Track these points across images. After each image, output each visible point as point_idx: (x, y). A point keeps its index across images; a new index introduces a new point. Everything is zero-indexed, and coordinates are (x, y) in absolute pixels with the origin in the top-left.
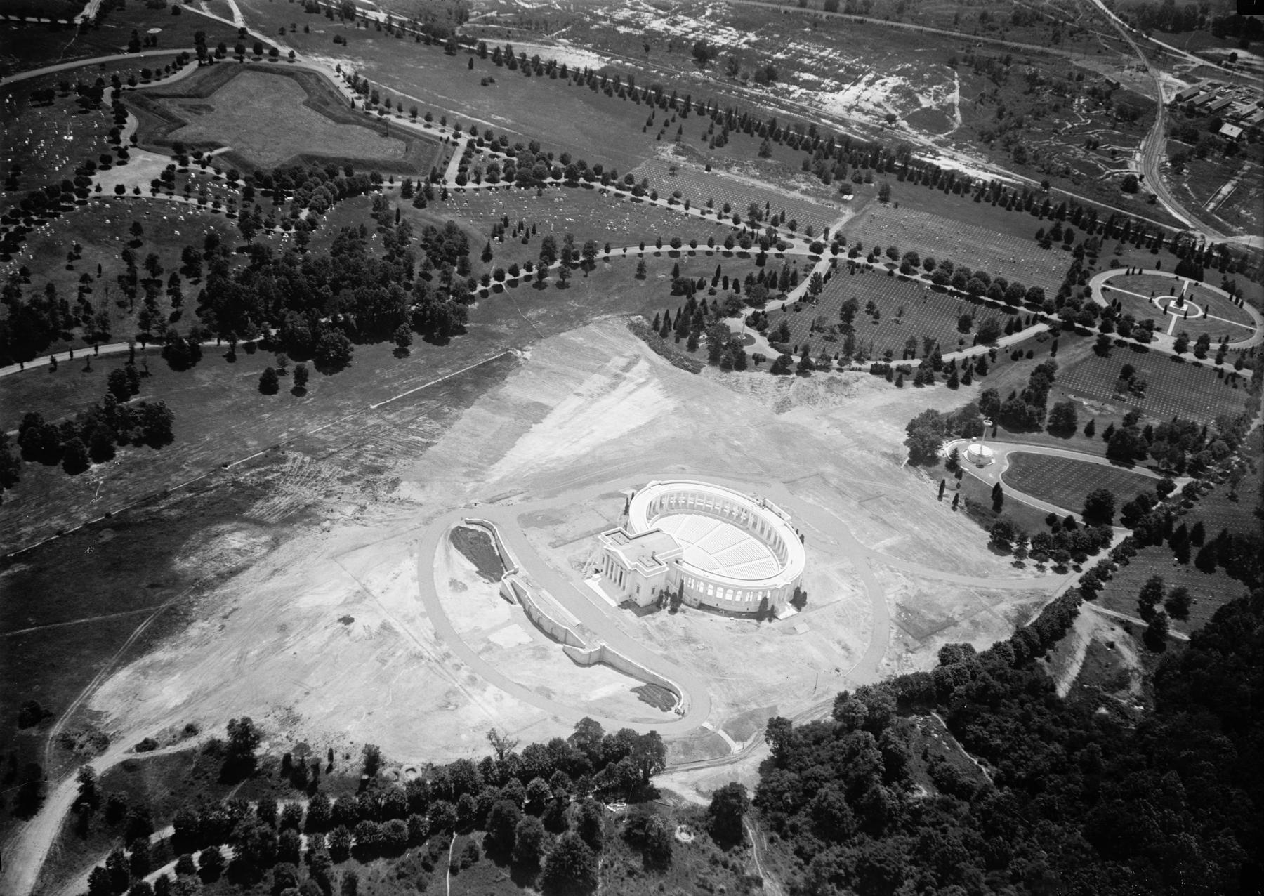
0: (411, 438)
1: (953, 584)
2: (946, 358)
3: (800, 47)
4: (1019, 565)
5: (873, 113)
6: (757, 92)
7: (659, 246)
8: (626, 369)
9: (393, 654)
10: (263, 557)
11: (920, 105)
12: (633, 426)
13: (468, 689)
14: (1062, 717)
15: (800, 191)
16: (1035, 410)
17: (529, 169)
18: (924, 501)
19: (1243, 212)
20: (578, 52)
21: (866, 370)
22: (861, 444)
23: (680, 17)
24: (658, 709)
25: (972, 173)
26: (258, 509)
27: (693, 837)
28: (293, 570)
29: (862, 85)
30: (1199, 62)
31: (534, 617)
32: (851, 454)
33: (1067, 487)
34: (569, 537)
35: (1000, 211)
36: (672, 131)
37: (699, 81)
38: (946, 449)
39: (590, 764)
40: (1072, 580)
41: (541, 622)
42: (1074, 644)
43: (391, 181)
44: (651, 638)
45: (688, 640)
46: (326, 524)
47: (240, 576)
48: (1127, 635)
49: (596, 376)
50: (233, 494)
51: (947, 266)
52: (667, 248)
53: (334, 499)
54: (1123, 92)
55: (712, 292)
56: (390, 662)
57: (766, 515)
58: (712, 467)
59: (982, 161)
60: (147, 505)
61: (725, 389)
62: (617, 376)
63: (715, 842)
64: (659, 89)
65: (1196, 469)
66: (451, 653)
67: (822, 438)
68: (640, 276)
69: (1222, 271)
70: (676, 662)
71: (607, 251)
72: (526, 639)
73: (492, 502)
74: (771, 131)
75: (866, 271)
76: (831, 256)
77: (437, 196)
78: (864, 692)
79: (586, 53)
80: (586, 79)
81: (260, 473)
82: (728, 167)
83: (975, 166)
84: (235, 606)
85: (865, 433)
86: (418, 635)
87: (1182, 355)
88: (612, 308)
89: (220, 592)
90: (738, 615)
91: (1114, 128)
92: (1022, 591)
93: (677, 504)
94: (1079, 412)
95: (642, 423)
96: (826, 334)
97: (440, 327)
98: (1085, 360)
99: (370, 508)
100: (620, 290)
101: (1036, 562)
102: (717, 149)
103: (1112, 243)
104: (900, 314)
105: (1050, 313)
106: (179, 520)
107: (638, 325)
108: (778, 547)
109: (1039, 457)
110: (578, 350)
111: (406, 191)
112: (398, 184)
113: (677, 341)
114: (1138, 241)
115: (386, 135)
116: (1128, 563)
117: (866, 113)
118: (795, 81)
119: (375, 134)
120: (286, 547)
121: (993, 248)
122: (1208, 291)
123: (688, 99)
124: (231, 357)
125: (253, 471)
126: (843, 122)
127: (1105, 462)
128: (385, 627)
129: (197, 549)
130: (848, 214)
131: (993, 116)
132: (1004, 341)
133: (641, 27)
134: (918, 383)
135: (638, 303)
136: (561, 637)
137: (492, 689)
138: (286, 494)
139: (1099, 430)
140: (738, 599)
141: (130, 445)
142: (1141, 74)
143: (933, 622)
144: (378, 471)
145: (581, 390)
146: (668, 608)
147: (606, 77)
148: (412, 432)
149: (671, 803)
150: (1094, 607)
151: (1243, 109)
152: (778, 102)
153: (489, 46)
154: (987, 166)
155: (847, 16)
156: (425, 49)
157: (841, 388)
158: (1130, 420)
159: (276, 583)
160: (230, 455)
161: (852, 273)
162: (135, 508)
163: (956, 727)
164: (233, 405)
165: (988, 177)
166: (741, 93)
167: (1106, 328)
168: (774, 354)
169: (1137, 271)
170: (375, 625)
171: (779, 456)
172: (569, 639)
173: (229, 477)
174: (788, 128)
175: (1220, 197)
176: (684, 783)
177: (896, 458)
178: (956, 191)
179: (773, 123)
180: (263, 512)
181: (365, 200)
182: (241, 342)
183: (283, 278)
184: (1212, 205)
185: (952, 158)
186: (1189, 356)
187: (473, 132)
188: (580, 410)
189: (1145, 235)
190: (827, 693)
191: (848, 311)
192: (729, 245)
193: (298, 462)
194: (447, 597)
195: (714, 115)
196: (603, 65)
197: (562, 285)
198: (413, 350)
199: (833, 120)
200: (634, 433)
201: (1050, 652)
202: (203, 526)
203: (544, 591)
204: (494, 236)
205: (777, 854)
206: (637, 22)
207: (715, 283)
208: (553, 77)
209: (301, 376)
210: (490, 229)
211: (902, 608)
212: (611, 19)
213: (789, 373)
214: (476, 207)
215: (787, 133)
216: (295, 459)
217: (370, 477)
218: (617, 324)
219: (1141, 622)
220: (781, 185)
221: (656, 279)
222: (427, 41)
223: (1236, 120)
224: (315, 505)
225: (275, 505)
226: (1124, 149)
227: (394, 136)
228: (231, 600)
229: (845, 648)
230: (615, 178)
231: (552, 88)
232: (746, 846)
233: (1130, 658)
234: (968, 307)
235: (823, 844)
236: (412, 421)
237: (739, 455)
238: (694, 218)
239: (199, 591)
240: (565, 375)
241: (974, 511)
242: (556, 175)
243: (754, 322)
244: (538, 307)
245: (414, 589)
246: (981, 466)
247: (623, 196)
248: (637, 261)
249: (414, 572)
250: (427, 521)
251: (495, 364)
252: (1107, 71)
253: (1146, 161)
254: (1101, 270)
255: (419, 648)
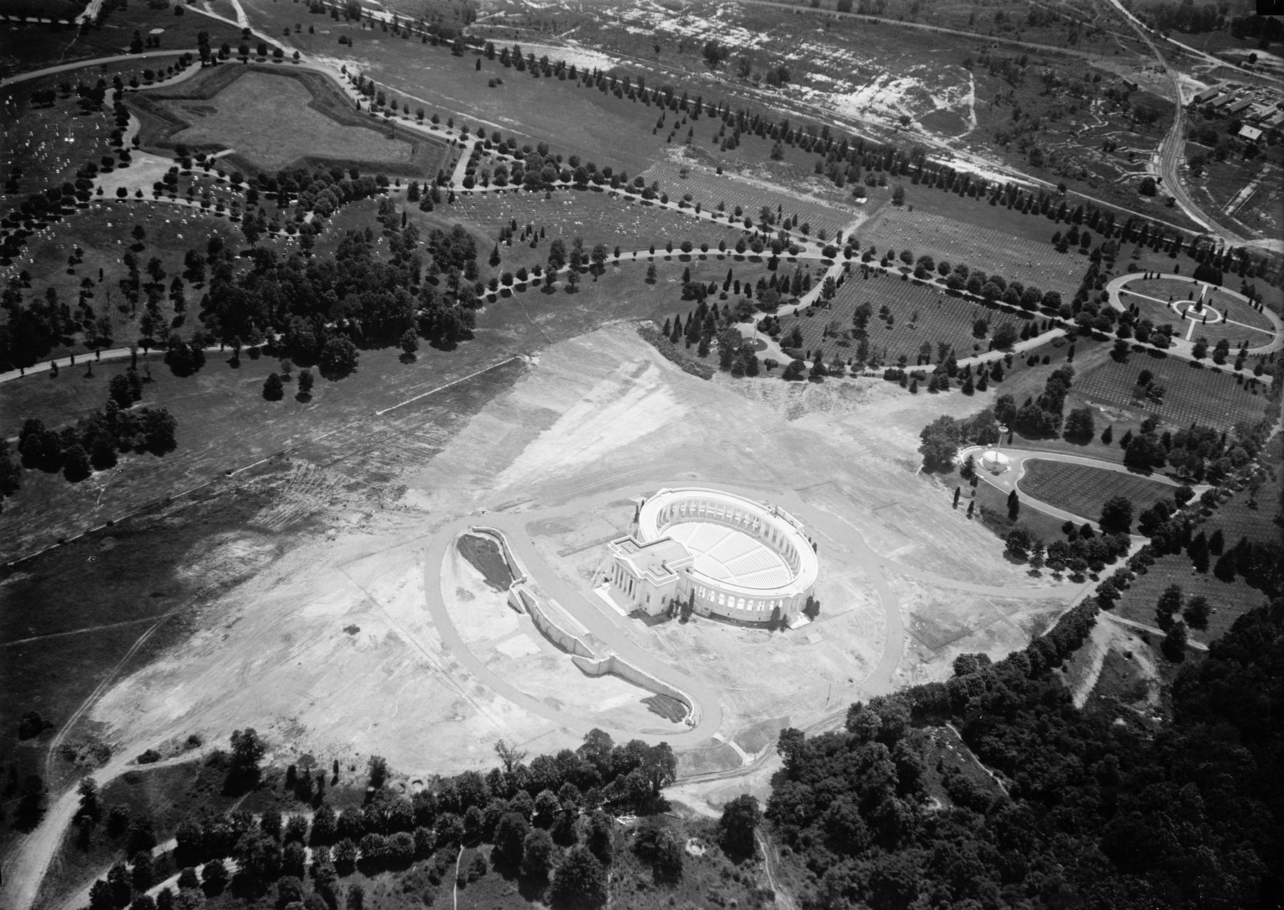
0: (417, 445)
1: (968, 594)
2: (961, 364)
3: (812, 48)
4: (1035, 574)
5: (887, 114)
6: (769, 93)
7: (669, 250)
8: (636, 375)
9: (399, 664)
10: (267, 566)
11: (934, 107)
12: (643, 433)
13: (475, 700)
14: (1079, 729)
15: (813, 194)
16: (1052, 416)
17: (537, 172)
18: (939, 509)
19: (1263, 215)
20: (587, 52)
21: (879, 376)
22: (875, 451)
23: (691, 18)
24: (668, 720)
25: (987, 175)
26: (262, 517)
27: (704, 850)
28: (297, 579)
29: (875, 87)
30: (1218, 63)
31: (543, 627)
32: (865, 461)
33: (1084, 495)
34: (578, 545)
35: (1016, 214)
36: (683, 133)
37: (710, 82)
38: (961, 456)
39: (599, 776)
40: (1089, 589)
41: (550, 632)
42: (1091, 654)
43: (398, 184)
44: (661, 648)
45: (699, 650)
46: (332, 532)
47: (244, 585)
48: (1145, 645)
49: (606, 382)
50: (236, 502)
51: (962, 270)
52: (677, 252)
53: (340, 507)
54: (1141, 93)
55: (723, 297)
56: (397, 673)
57: (778, 523)
58: (723, 475)
59: (997, 164)
60: (149, 513)
61: (736, 395)
62: (626, 382)
63: (726, 855)
64: (669, 91)
65: (1215, 476)
66: (458, 663)
67: (835, 445)
68: (650, 281)
69: (1241, 275)
70: (687, 673)
71: (617, 255)
72: (534, 649)
73: (499, 509)
74: (784, 133)
75: (880, 276)
76: (845, 260)
77: (444, 199)
78: (877, 703)
79: (595, 53)
80: (595, 80)
81: (264, 480)
82: (739, 170)
83: (991, 168)
84: (239, 615)
85: (879, 440)
86: (425, 645)
87: (1201, 361)
88: (622, 313)
89: (223, 601)
90: (750, 624)
91: (1131, 130)
92: (1038, 600)
93: (688, 512)
94: (1096, 419)
95: (652, 430)
96: (839, 339)
97: (447, 332)
98: (1102, 365)
99: (376, 516)
100: (630, 295)
101: (1052, 571)
102: (728, 151)
103: (1130, 247)
104: (915, 319)
105: (1067, 318)
106: (182, 528)
107: (648, 330)
108: (790, 556)
109: (1055, 464)
110: (587, 355)
111: (413, 194)
112: (404, 187)
113: (688, 346)
114: (1156, 244)
115: (392, 137)
116: (1145, 572)
117: (880, 115)
118: (807, 82)
119: (381, 136)
120: (290, 556)
121: (1009, 252)
122: (1227, 296)
123: (699, 100)
124: (234, 363)
125: (257, 479)
126: (857, 124)
127: (1122, 469)
128: (391, 637)
129: (200, 557)
130: (862, 217)
131: (1008, 118)
132: (1020, 347)
133: (651, 28)
134: (932, 389)
135: (648, 308)
136: (570, 646)
137: (500, 700)
138: (291, 502)
139: (1117, 437)
140: (749, 608)
141: (132, 452)
142: (1159, 75)
143: (947, 631)
144: (384, 478)
145: (590, 396)
146: (679, 617)
147: (615, 78)
148: (418, 439)
149: (681, 815)
150: (1111, 616)
151: (1262, 110)
152: (790, 104)
153: (497, 47)
154: (1002, 169)
155: (861, 16)
156: (432, 50)
157: (854, 394)
158: (1148, 427)
159: (280, 592)
160: (234, 462)
161: (866, 278)
162: (137, 516)
163: (971, 738)
164: (236, 412)
165: (1003, 180)
166: (753, 94)
167: (1123, 333)
168: (786, 360)
169: (1155, 276)
170: (381, 635)
171: (791, 463)
172: (578, 649)
173: (232, 485)
174: (801, 130)
175: (1239, 200)
176: (695, 796)
177: (910, 466)
178: (972, 194)
179: (785, 125)
180: (267, 520)
181: (371, 203)
182: (245, 347)
183: (287, 283)
184: (1231, 208)
185: (967, 160)
186: (1208, 362)
187: (481, 134)
188: (589, 416)
189: (1163, 239)
190: (840, 703)
191: (862, 315)
192: (740, 248)
193: (303, 469)
194: (454, 607)
195: (725, 116)
196: (613, 66)
197: (570, 290)
198: (419, 356)
199: (846, 122)
200: (644, 439)
201: (1066, 662)
202: (206, 534)
203: (553, 601)
204: (501, 240)
205: (789, 868)
206: (648, 23)
207: (726, 287)
208: (562, 78)
209: (306, 382)
210: (497, 232)
211: (916, 618)
212: (621, 19)
213: (801, 378)
214: (483, 210)
215: (799, 136)
216: (300, 466)
217: (376, 484)
218: (627, 329)
219: (1159, 632)
220: (793, 188)
221: (666, 284)
222: (434, 42)
223: (1256, 122)
224: (320, 513)
225: (279, 513)
226: (1142, 151)
227: (401, 138)
228: (234, 609)
229: (859, 658)
230: (624, 181)
231: (561, 90)
232: (758, 860)
233: (1148, 668)
234: (983, 312)
235: (836, 857)
236: (418, 428)
237: (750, 462)
238: (705, 221)
239: (202, 600)
240: (574, 380)
241: (990, 519)
242: (565, 178)
243: (766, 327)
244: (546, 312)
245: (421, 599)
246: (997, 474)
247: (633, 199)
248: (647, 265)
249: (421, 581)
250: (434, 529)
251: (503, 370)
252: (1125, 72)
253: (1164, 163)
254: (1118, 275)
255: (426, 658)
